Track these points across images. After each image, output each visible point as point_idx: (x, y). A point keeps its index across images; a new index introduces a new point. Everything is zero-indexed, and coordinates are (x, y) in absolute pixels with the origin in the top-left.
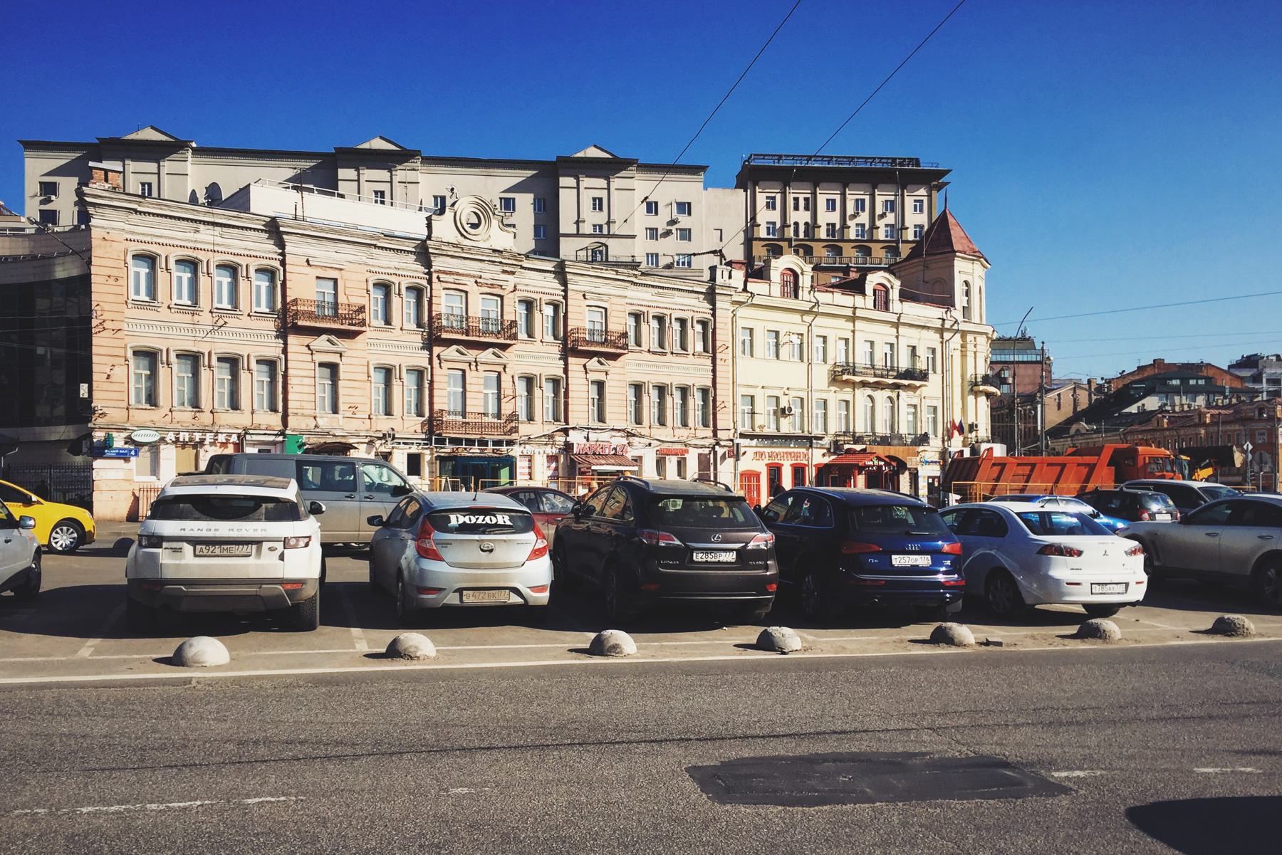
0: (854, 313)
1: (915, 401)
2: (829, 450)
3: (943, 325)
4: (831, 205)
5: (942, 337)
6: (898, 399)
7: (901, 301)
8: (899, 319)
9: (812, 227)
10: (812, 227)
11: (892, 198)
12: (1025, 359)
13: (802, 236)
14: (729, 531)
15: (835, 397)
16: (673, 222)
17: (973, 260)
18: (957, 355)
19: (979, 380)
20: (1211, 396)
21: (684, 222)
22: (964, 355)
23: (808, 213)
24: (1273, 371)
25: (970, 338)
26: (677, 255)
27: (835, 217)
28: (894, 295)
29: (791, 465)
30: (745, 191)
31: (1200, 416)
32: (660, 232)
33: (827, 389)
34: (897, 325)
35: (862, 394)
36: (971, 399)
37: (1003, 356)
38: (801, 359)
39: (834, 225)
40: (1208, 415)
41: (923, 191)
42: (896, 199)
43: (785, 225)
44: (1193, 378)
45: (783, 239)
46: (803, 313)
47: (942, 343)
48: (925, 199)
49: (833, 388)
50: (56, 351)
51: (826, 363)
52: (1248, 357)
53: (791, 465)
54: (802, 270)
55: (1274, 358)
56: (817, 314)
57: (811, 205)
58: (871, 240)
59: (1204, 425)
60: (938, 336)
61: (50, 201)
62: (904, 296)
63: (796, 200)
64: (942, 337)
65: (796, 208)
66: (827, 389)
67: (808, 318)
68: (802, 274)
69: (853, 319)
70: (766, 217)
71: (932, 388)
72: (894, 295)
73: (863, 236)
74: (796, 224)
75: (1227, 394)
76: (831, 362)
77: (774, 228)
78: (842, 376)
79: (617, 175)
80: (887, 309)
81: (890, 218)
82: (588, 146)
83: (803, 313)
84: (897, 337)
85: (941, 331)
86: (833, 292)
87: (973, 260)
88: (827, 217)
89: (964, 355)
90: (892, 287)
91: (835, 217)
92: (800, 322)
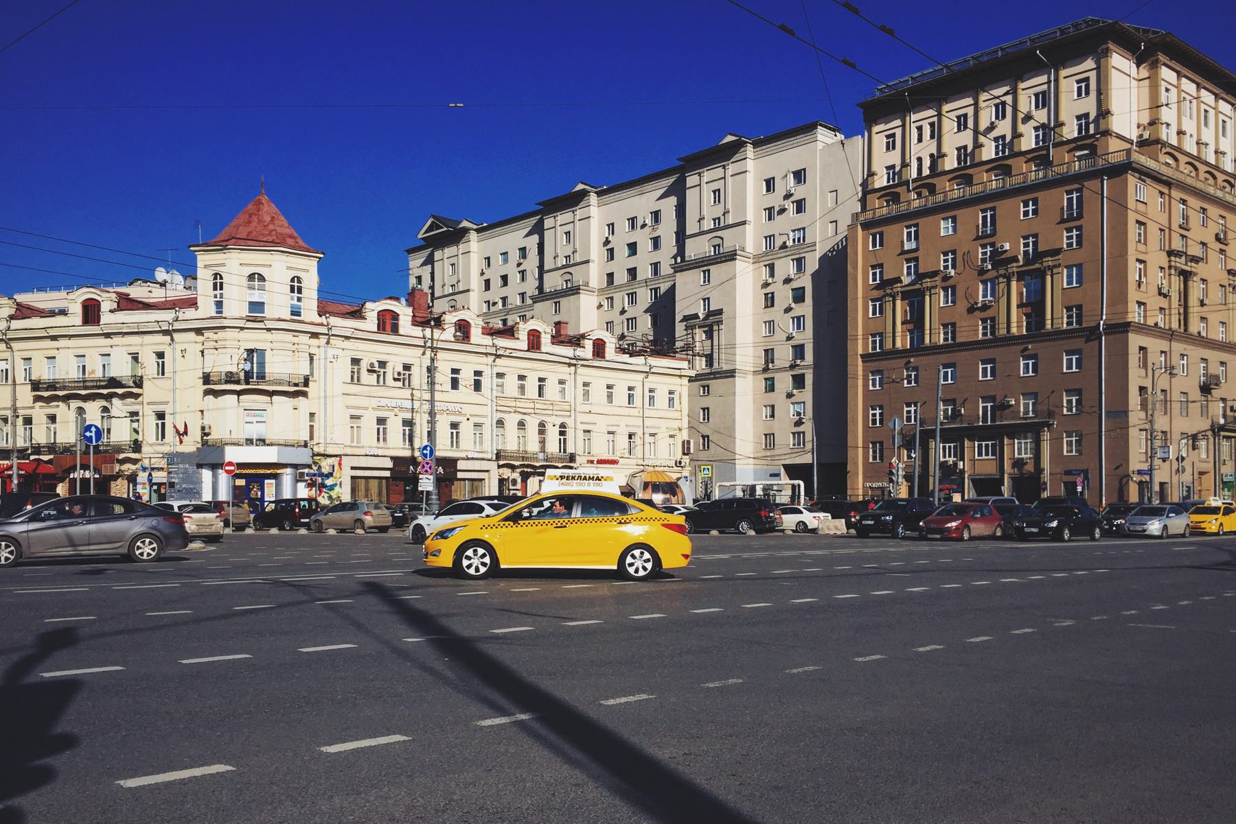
4: (962, 123)
9: (937, 158)
10: (937, 158)
11: (1045, 87)
12: (897, 334)
13: (926, 172)
14: (72, 525)
15: (39, 413)
16: (788, 196)
21: (799, 193)
23: (934, 142)
26: (794, 231)
27: (966, 138)
30: (863, 137)
32: (777, 209)
37: (900, 334)
39: (965, 147)
41: (1090, 64)
42: (1049, 87)
43: (905, 165)
45: (900, 185)
48: (1093, 76)
50: (1065, 436)
57: (936, 133)
58: (973, 166)
63: (920, 129)
65: (920, 140)
70: (883, 159)
73: (894, 181)
74: (920, 160)
77: (894, 173)
79: (732, 160)
81: (1041, 116)
82: (725, 136)
88: (954, 139)
91: (966, 138)
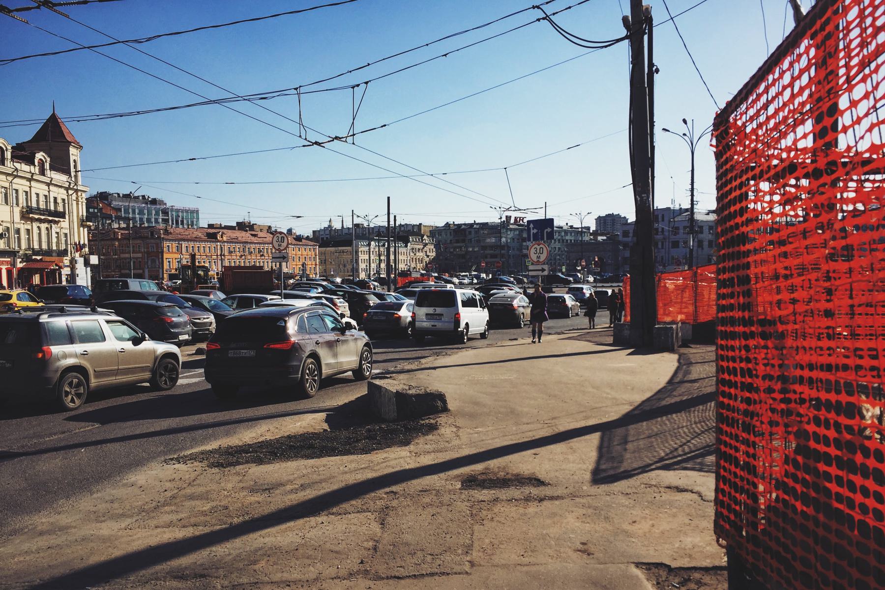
0: (32, 176)
1: (58, 230)
2: (22, 259)
3: (69, 186)
5: (68, 193)
6: (51, 229)
7: (51, 171)
8: (51, 181)
15: (23, 227)
17: (78, 148)
18: (74, 203)
19: (85, 218)
20: (104, 221)
22: (77, 204)
24: (117, 204)
25: (79, 194)
28: (47, 166)
29: (6, 269)
31: (114, 235)
33: (19, 221)
34: (48, 185)
35: (35, 225)
36: (82, 229)
38: (6, 203)
40: (120, 234)
44: (92, 208)
46: (7, 174)
47: (68, 196)
49: (23, 222)
51: (18, 206)
52: (102, 193)
53: (6, 269)
54: (6, 148)
55: (116, 195)
56: (16, 176)
59: (117, 239)
60: (65, 192)
61: (851, 368)
62: (52, 168)
64: (68, 193)
66: (19, 221)
67: (10, 178)
68: (7, 150)
69: (30, 180)
71: (65, 224)
72: (47, 166)
75: (114, 219)
76: (21, 206)
78: (27, 214)
80: (44, 175)
83: (7, 174)
84: (49, 192)
85: (67, 189)
86: (21, 163)
87: (78, 148)
89: (77, 204)
90: (46, 162)
92: (5, 180)
